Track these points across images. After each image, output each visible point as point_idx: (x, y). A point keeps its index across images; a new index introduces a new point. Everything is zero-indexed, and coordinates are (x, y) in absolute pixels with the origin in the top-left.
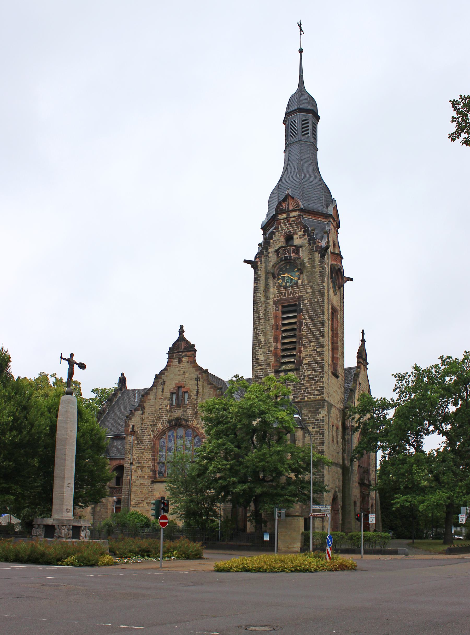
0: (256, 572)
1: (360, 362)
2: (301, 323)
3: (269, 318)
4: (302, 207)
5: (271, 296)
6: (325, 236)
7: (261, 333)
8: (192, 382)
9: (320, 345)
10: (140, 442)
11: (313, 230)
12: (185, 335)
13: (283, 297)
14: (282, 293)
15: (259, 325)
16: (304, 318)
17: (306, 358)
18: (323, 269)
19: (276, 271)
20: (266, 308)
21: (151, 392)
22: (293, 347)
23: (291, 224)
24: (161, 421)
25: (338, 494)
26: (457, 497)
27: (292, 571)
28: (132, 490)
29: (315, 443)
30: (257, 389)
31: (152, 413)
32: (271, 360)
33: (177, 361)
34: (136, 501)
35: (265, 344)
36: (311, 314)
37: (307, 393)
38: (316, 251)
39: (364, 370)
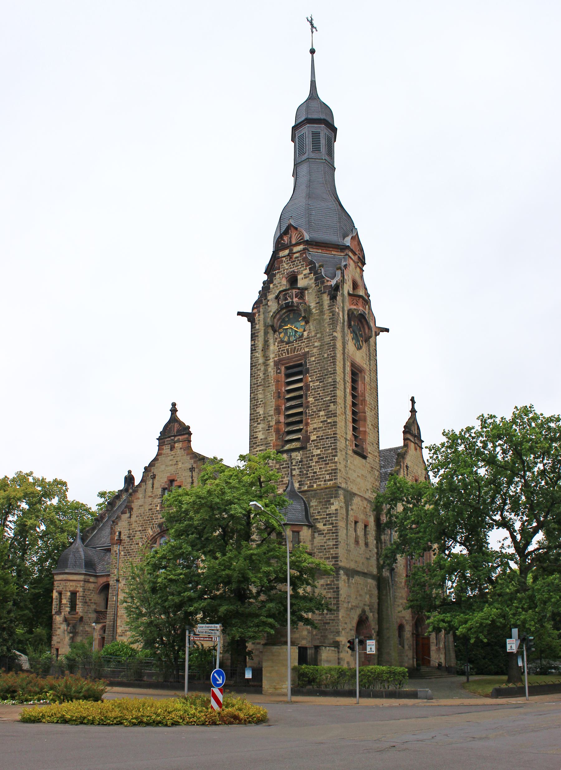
0: (77, 725)
1: (408, 439)
2: (307, 387)
3: (269, 383)
4: (307, 237)
5: (272, 356)
6: (339, 273)
7: (260, 404)
8: (186, 474)
9: (332, 414)
10: (128, 553)
11: (321, 266)
12: (179, 415)
13: (286, 355)
14: (284, 350)
15: (257, 394)
16: (310, 380)
17: (314, 433)
18: (333, 315)
19: (277, 323)
20: (266, 370)
21: (139, 489)
22: (299, 419)
23: (295, 261)
24: (150, 525)
25: (370, 615)
26: (514, 615)
27: (134, 725)
28: (118, 614)
29: (327, 545)
30: (234, 473)
31: (141, 516)
32: (272, 439)
33: (168, 449)
34: (123, 629)
35: (264, 417)
36: (320, 374)
37: (316, 479)
38: (325, 293)
39: (416, 449)
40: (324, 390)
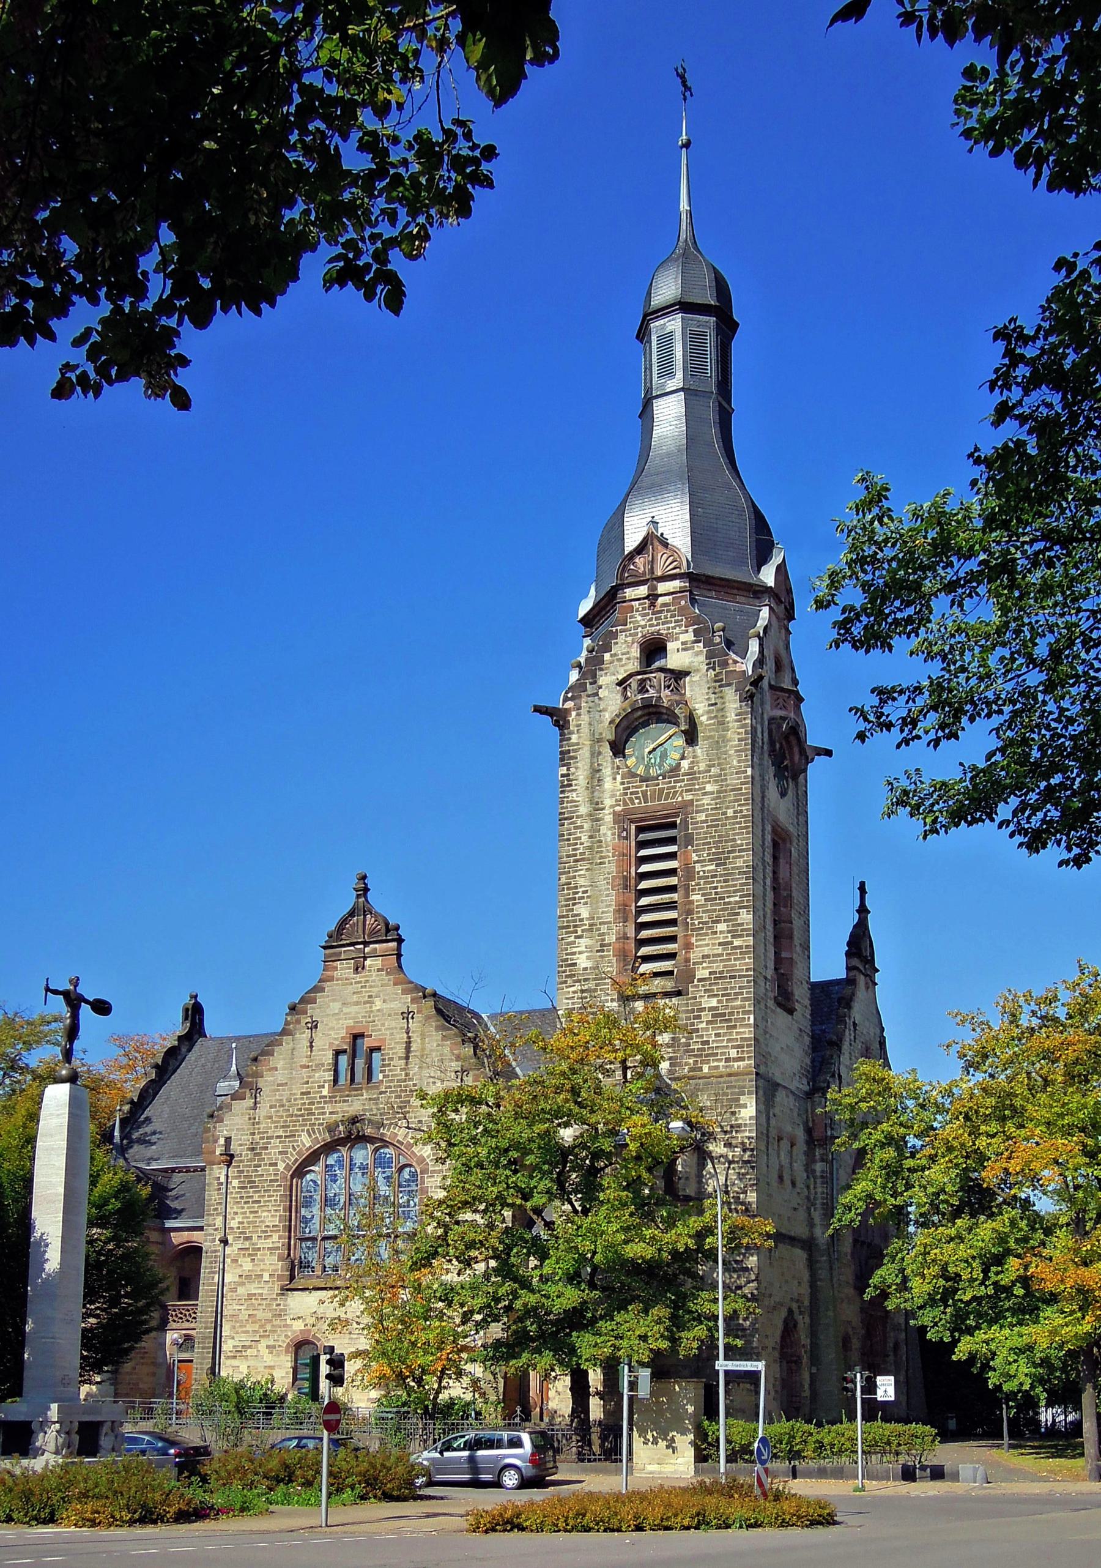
2: (690, 873)
5: (608, 802)
8: (393, 1024)
9: (742, 930)
14: (637, 793)
15: (575, 877)
16: (696, 859)
17: (704, 965)
23: (661, 612)
33: (349, 968)
36: (716, 848)
39: (867, 988)
40: (726, 881)
